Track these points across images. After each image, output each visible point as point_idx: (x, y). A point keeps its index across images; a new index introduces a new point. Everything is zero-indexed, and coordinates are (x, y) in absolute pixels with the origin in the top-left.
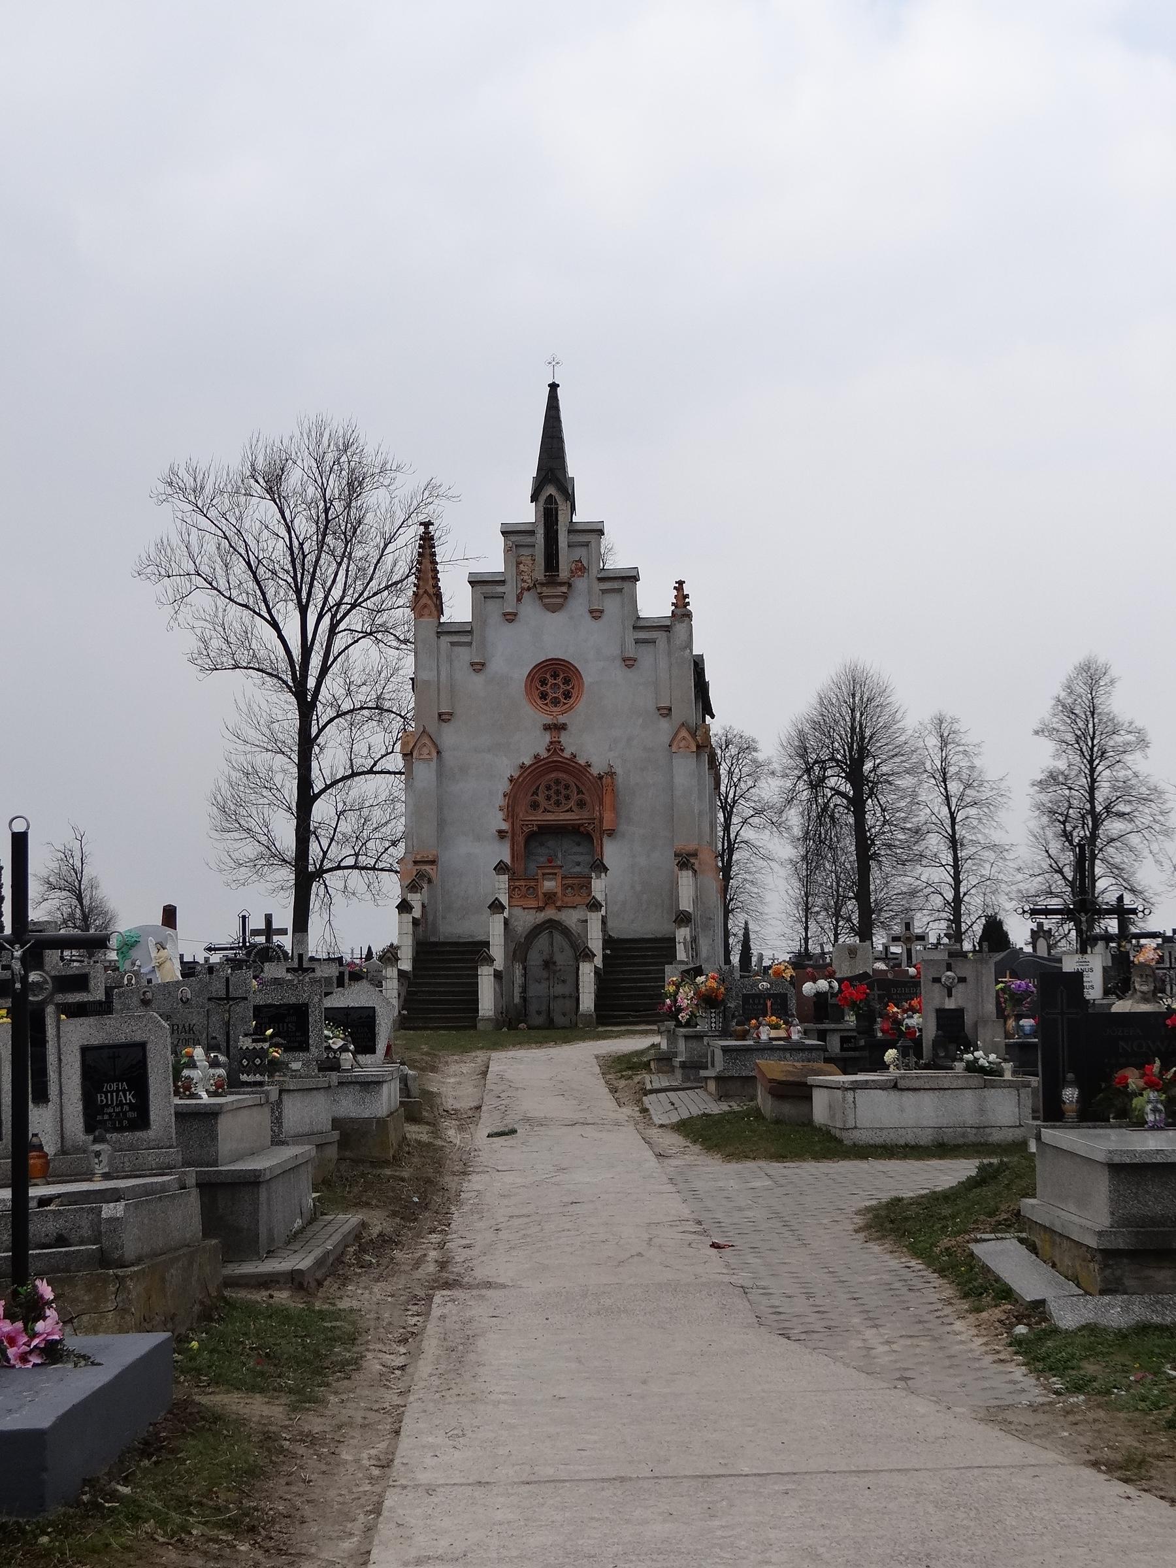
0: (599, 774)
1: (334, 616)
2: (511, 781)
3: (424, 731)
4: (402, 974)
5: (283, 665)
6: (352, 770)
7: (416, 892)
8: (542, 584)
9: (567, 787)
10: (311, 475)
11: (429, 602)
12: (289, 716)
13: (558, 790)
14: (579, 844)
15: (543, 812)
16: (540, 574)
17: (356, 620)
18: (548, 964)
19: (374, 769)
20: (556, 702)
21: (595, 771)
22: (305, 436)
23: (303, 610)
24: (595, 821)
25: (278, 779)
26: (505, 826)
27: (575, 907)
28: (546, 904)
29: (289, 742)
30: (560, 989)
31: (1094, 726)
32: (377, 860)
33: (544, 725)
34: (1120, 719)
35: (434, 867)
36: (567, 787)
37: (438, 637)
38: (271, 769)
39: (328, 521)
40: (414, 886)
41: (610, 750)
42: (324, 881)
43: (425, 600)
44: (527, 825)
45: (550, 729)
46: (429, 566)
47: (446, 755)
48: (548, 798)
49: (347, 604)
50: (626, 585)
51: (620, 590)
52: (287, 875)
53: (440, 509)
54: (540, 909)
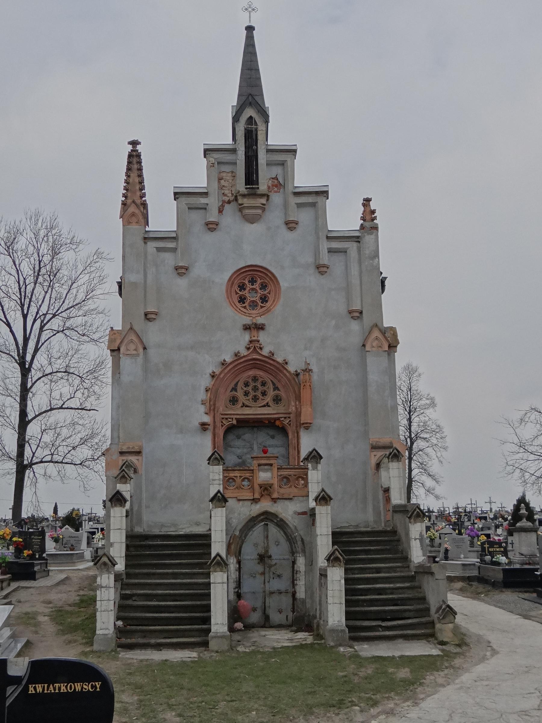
0: (296, 371)
1: (42, 322)
2: (213, 377)
3: (131, 328)
4: (118, 577)
5: (13, 347)
6: (51, 407)
7: (125, 483)
8: (244, 196)
10: (32, 243)
11: (137, 211)
12: (16, 375)
13: (255, 386)
14: (273, 437)
15: (242, 407)
16: (241, 186)
17: (55, 324)
18: (263, 558)
19: (63, 406)
20: (253, 305)
21: (292, 368)
22: (28, 220)
23: (25, 317)
24: (291, 416)
25: (8, 411)
26: (207, 419)
27: (291, 499)
28: (262, 496)
29: (15, 390)
30: (276, 585)
31: (411, 396)
32: (64, 457)
33: (244, 325)
34: (423, 393)
35: (139, 458)
36: (264, 384)
37: (145, 243)
38: (4, 405)
39: (40, 268)
40: (123, 477)
41: (306, 349)
42: (33, 470)
43: (132, 209)
44: (227, 419)
45: (250, 328)
46: (137, 180)
47: (151, 352)
48: (246, 394)
49: (50, 314)
51: (313, 205)
52: (12, 466)
53: (102, 265)
54: (255, 501)
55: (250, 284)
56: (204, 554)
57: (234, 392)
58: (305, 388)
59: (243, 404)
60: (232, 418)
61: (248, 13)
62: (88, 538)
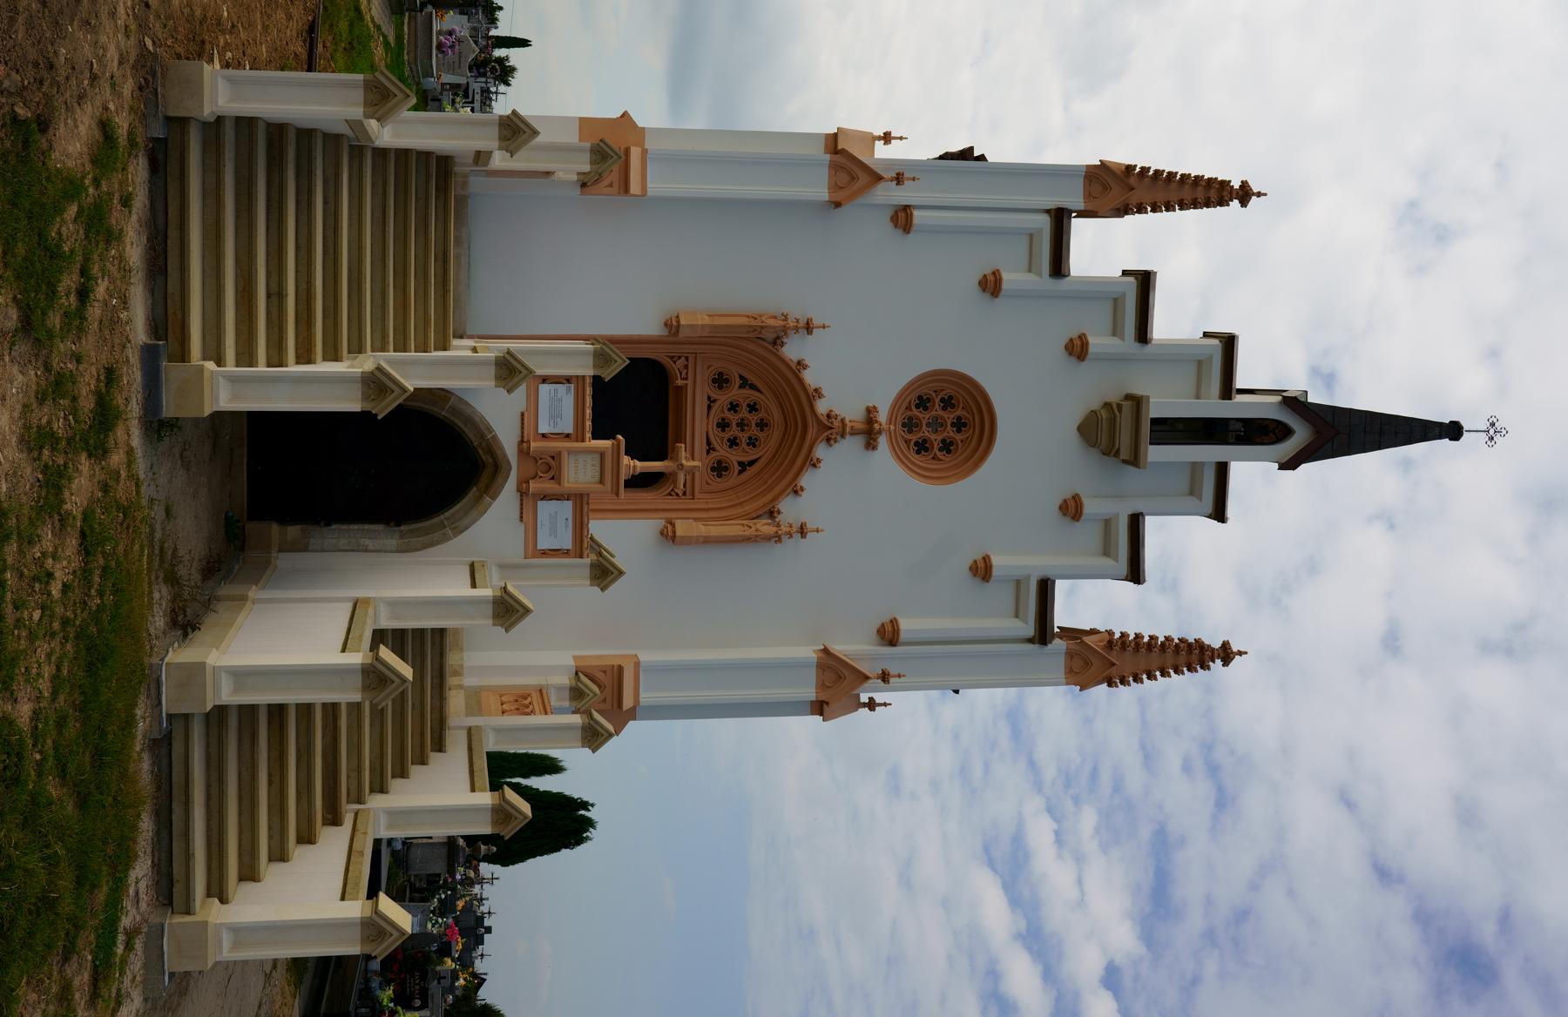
0: (779, 513)
9: (752, 442)
44: (686, 367)
50: (1123, 565)
55: (955, 421)
56: (384, 336)
57: (738, 382)
58: (746, 528)
59: (715, 401)
60: (686, 379)
61: (1485, 428)
62: (458, 86)
